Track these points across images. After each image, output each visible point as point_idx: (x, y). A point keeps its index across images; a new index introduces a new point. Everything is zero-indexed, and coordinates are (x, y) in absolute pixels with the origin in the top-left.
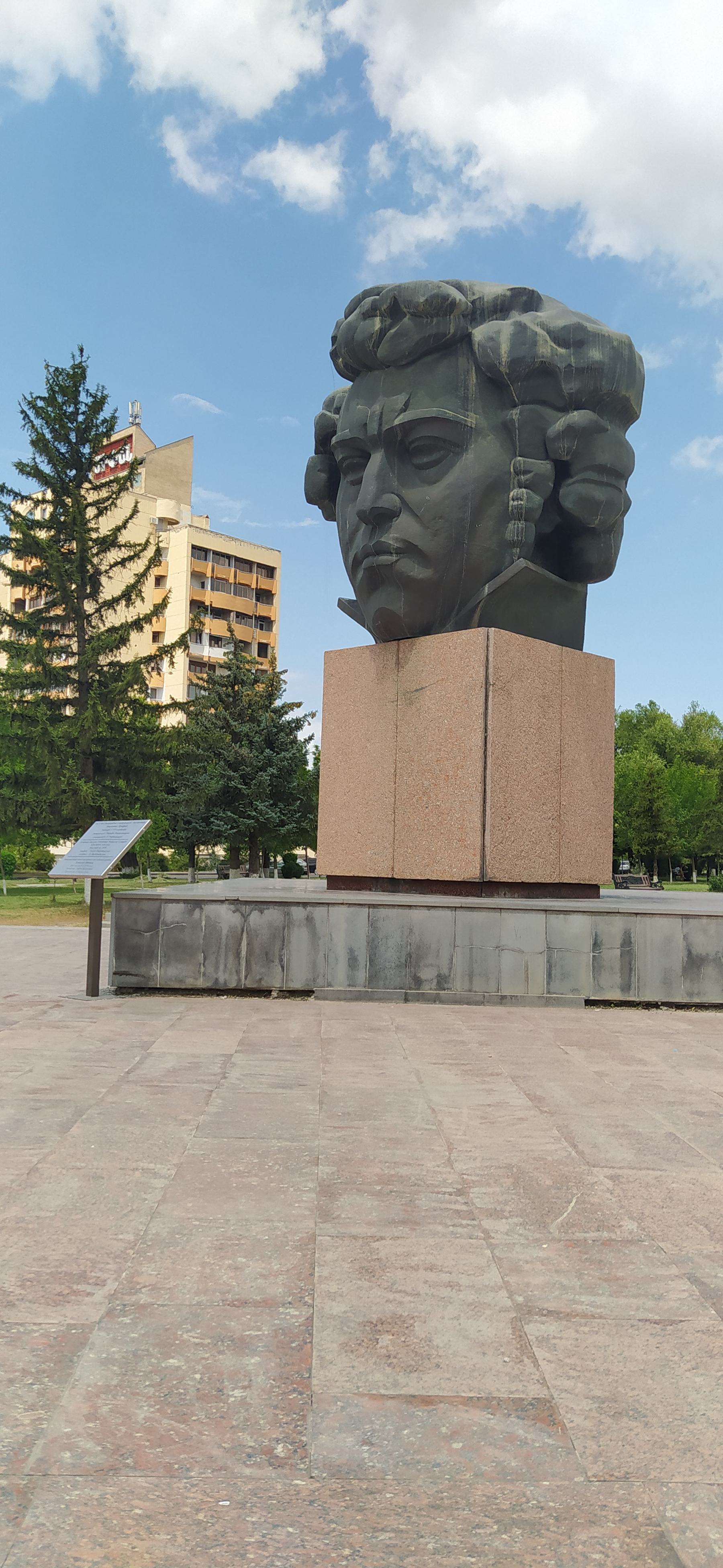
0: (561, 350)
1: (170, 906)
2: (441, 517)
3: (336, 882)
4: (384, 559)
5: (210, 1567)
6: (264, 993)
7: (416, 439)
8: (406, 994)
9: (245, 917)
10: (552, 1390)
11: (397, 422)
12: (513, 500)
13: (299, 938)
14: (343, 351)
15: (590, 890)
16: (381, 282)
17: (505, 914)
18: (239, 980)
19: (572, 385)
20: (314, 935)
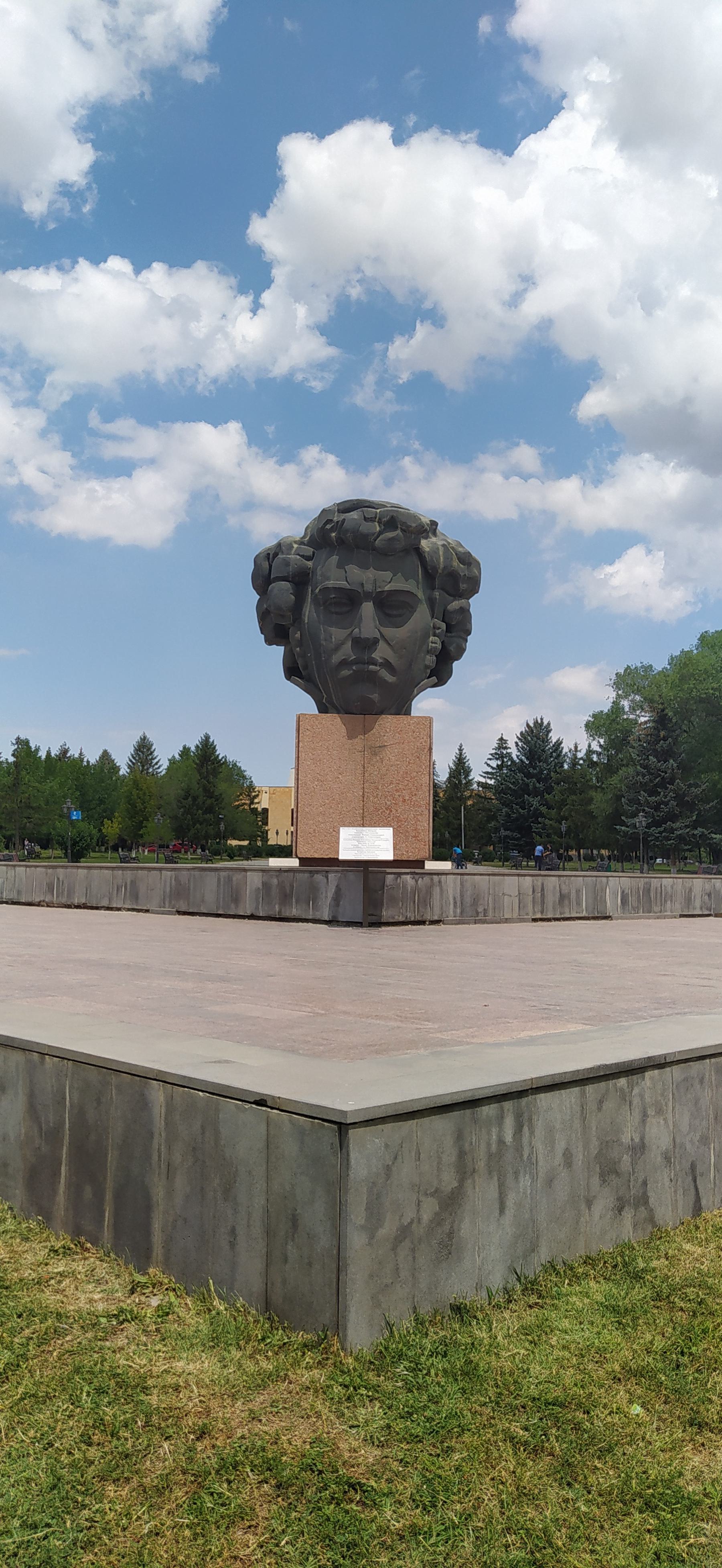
0: (461, 566)
1: (389, 876)
3: (304, 861)
5: (1, 1411)
6: (422, 923)
9: (417, 881)
10: (90, 1254)
11: (386, 589)
12: (432, 643)
13: (437, 891)
18: (415, 916)
19: (465, 585)
20: (441, 890)
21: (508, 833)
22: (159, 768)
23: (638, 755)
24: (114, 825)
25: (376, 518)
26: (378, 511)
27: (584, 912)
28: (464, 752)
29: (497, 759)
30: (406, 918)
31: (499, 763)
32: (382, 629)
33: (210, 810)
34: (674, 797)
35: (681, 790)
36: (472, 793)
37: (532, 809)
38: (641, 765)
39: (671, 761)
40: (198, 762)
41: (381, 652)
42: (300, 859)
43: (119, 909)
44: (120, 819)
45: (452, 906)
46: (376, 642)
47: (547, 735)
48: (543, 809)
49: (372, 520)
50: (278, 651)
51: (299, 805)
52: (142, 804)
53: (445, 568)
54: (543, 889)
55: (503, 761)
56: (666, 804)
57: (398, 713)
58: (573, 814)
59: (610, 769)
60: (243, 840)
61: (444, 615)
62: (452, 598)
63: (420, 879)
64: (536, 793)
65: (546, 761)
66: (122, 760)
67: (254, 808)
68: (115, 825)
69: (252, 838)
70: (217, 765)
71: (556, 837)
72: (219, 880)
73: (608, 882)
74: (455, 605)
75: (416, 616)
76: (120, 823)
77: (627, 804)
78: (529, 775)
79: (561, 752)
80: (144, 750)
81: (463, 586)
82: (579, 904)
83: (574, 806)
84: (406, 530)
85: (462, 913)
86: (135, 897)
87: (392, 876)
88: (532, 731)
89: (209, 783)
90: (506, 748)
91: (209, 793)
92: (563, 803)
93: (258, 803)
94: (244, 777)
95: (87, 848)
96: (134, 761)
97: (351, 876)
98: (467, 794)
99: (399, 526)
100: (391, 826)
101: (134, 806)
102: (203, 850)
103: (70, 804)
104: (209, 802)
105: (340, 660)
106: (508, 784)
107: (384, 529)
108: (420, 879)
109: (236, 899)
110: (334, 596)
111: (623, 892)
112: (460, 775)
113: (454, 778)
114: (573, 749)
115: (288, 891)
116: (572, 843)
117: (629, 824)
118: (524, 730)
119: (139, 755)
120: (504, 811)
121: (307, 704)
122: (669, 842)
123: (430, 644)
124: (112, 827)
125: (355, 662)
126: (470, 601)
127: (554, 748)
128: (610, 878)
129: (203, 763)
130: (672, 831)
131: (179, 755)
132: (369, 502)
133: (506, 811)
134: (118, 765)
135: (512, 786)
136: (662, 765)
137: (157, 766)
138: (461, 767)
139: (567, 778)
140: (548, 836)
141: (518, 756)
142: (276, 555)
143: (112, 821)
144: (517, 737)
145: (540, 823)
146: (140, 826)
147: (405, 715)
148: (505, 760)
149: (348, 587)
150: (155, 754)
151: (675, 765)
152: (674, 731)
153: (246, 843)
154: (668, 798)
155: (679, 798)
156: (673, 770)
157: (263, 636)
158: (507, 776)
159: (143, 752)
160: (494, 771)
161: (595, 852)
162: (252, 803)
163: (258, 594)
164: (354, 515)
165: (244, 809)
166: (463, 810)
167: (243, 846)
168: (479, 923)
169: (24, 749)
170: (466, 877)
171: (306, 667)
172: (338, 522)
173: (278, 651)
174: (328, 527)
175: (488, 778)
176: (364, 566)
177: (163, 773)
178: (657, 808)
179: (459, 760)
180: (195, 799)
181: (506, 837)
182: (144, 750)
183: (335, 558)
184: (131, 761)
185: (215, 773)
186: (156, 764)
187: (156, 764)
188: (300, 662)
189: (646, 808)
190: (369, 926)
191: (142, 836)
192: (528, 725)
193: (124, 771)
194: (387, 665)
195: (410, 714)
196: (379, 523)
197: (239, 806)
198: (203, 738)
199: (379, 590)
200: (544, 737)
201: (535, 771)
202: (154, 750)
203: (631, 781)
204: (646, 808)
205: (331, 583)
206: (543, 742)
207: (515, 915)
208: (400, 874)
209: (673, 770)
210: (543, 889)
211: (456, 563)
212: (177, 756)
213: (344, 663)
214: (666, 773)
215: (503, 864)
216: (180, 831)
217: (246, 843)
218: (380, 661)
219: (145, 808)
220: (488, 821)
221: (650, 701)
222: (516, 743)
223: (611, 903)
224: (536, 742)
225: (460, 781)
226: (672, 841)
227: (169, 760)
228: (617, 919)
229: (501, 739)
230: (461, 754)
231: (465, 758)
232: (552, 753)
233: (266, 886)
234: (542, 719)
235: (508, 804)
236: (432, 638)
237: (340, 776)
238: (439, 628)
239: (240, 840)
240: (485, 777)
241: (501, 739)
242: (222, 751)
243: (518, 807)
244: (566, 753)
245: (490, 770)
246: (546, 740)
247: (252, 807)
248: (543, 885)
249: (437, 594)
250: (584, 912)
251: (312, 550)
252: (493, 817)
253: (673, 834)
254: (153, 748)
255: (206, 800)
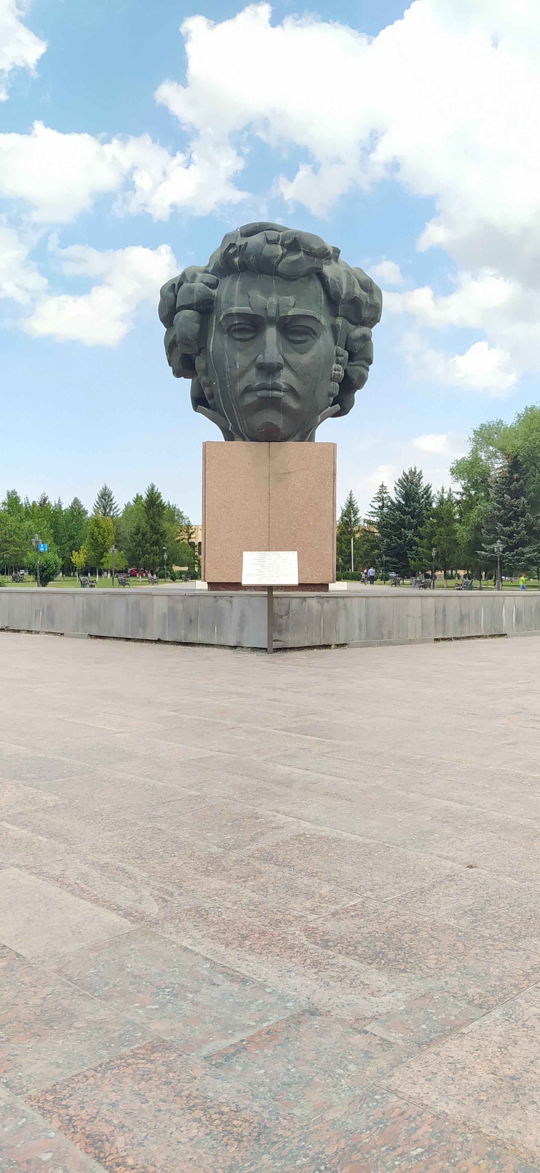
0: (364, 293)
2: (308, 375)
3: (213, 586)
4: (276, 393)
6: (327, 646)
7: (298, 326)
8: (380, 642)
9: (322, 605)
11: (290, 313)
12: (335, 370)
13: (342, 614)
14: (252, 258)
15: (324, 587)
16: (278, 221)
17: (410, 599)
18: (321, 641)
21: (388, 558)
22: (117, 511)
23: (495, 494)
24: (80, 556)
25: (278, 240)
26: (281, 234)
27: (483, 631)
28: (353, 496)
29: (379, 501)
30: (312, 643)
31: (381, 504)
32: (285, 355)
33: (156, 543)
34: (525, 527)
35: (530, 521)
36: (360, 527)
37: (407, 539)
38: (498, 502)
39: (523, 498)
40: (146, 506)
41: (285, 378)
42: (208, 583)
43: (37, 633)
44: (85, 551)
45: (357, 630)
46: (280, 368)
47: (419, 481)
48: (417, 539)
49: (274, 242)
50: (186, 384)
51: (207, 532)
52: (103, 539)
53: (347, 294)
54: (444, 610)
55: (383, 503)
56: (518, 533)
57: (302, 439)
58: (442, 542)
59: (468, 505)
60: (184, 566)
61: (346, 343)
62: (355, 326)
63: (326, 603)
64: (410, 527)
65: (418, 502)
66: (90, 505)
67: (191, 542)
68: (81, 556)
69: (191, 565)
70: (161, 508)
71: (427, 561)
72: (127, 604)
73: (504, 602)
74: (358, 332)
75: (320, 342)
76: (85, 554)
77: (486, 533)
78: (405, 513)
79: (430, 494)
80: (105, 497)
81: (366, 313)
82: (478, 622)
83: (441, 535)
84: (310, 253)
85: (367, 635)
86: (51, 620)
87: (298, 600)
88: (407, 478)
89: (155, 522)
90: (385, 493)
91: (155, 530)
92: (433, 534)
93: (195, 538)
94: (182, 517)
95: (55, 573)
96: (98, 506)
97: (256, 601)
98: (355, 529)
99: (302, 248)
100: (295, 550)
101: (96, 540)
102: (152, 575)
103: (37, 538)
104: (155, 537)
105: (244, 387)
106: (389, 520)
107: (287, 253)
108: (326, 603)
109: (144, 624)
110: (237, 322)
111: (517, 611)
112: (350, 514)
113: (346, 516)
114: (441, 491)
115: (193, 617)
116: (440, 566)
117: (487, 549)
118: (401, 478)
119: (102, 502)
120: (385, 541)
121: (215, 434)
122: (520, 564)
123: (334, 372)
124: (79, 557)
125: (261, 388)
126: (372, 330)
127: (425, 491)
128: (506, 598)
129: (150, 507)
130: (523, 554)
131: (134, 501)
132: (271, 224)
133: (386, 541)
134: (66, 506)
135: (392, 522)
136: (515, 501)
137: (116, 510)
138: (351, 508)
139: (436, 514)
140: (421, 560)
141: (396, 498)
142: (180, 284)
143: (79, 553)
144: (396, 483)
145: (414, 550)
146: (102, 555)
147: (308, 441)
148: (385, 502)
149: (252, 312)
150: (114, 501)
151: (526, 501)
152: (524, 474)
153: (186, 569)
154: (520, 528)
155: (528, 527)
156: (524, 505)
157: (171, 368)
158: (387, 514)
159: (105, 499)
160: (377, 511)
161: (454, 572)
162: (190, 538)
163: (166, 327)
164: (258, 238)
165: (184, 543)
166: (352, 541)
167: (183, 571)
168: (383, 645)
169: (13, 500)
170: (371, 600)
171: (212, 396)
172: (240, 246)
173: (186, 384)
174: (231, 251)
175: (372, 516)
176: (267, 293)
177: (121, 515)
178: (510, 536)
179: (350, 502)
180: (144, 535)
181: (387, 561)
182: (105, 497)
183: (238, 284)
184: (96, 506)
185: (160, 514)
186: (115, 508)
187: (115, 508)
188: (206, 391)
189: (502, 537)
190: (275, 652)
191: (102, 564)
192: (404, 474)
193: (91, 513)
194: (291, 390)
195: (314, 441)
196: (282, 245)
197: (179, 541)
198: (150, 487)
199: (282, 315)
200: (417, 482)
201: (410, 510)
202: (114, 497)
203: (490, 515)
204: (502, 537)
205: (234, 309)
206: (416, 486)
207: (418, 636)
208: (304, 598)
209: (524, 505)
210: (444, 610)
211: (358, 291)
212: (132, 503)
213: (248, 390)
214: (518, 508)
215: (385, 583)
216: (133, 560)
217: (186, 569)
218: (284, 386)
219: (105, 542)
220: (372, 549)
221: (502, 450)
222: (395, 488)
223: (507, 622)
224: (411, 487)
225: (350, 520)
226: (523, 563)
227: (125, 505)
228: (512, 636)
229: (382, 486)
230: (351, 498)
231: (354, 501)
232: (423, 495)
233: (172, 611)
234: (415, 468)
235: (389, 536)
236: (335, 366)
237: (246, 503)
238: (342, 356)
239: (181, 566)
240: (369, 516)
241: (382, 486)
242: (166, 498)
243: (396, 538)
244: (434, 495)
245: (374, 510)
246: (418, 485)
247: (190, 541)
248: (444, 607)
249: (340, 321)
250: (483, 631)
251: (216, 277)
252: (377, 547)
253: (523, 557)
254: (112, 495)
255: (152, 535)
